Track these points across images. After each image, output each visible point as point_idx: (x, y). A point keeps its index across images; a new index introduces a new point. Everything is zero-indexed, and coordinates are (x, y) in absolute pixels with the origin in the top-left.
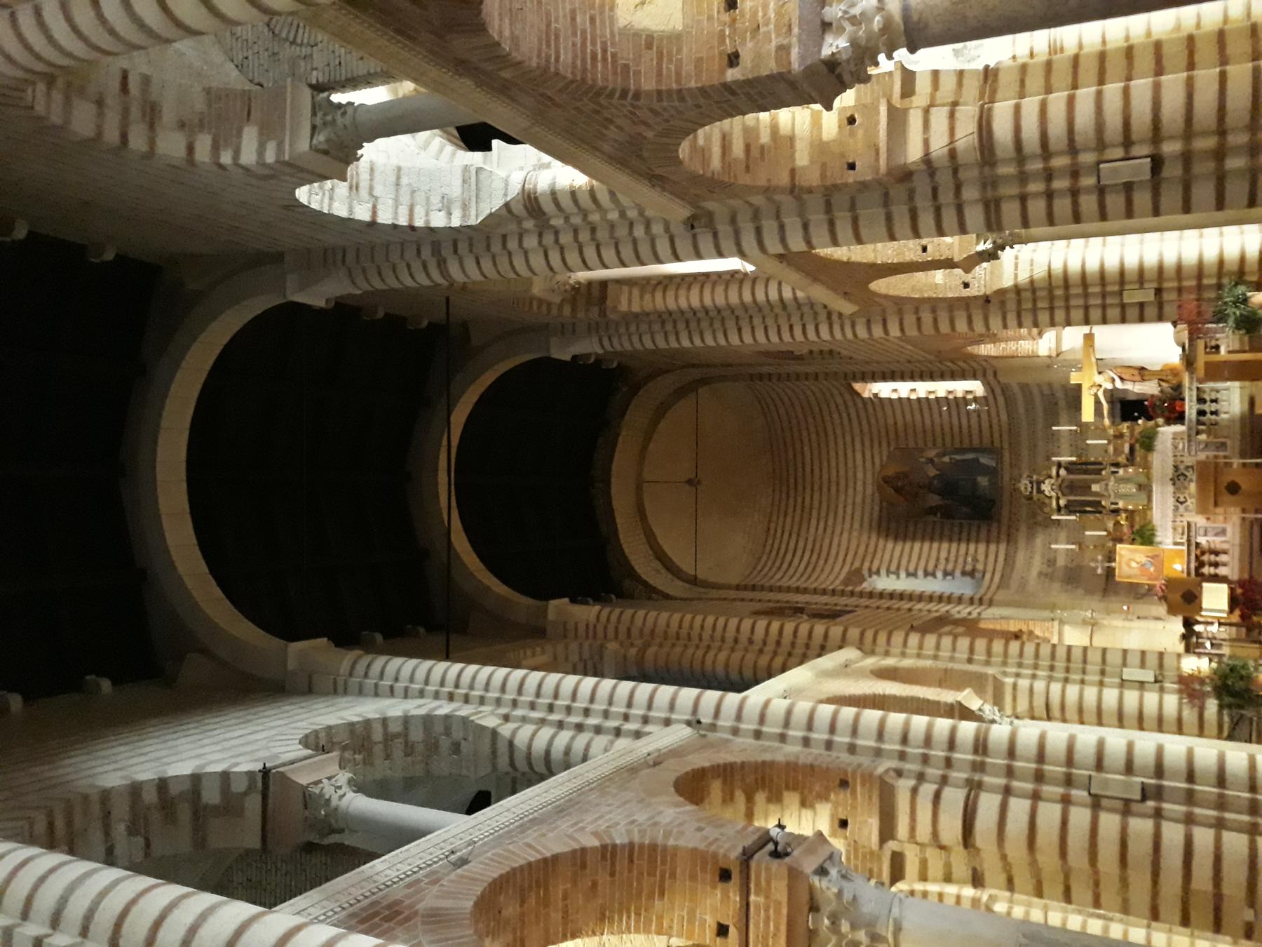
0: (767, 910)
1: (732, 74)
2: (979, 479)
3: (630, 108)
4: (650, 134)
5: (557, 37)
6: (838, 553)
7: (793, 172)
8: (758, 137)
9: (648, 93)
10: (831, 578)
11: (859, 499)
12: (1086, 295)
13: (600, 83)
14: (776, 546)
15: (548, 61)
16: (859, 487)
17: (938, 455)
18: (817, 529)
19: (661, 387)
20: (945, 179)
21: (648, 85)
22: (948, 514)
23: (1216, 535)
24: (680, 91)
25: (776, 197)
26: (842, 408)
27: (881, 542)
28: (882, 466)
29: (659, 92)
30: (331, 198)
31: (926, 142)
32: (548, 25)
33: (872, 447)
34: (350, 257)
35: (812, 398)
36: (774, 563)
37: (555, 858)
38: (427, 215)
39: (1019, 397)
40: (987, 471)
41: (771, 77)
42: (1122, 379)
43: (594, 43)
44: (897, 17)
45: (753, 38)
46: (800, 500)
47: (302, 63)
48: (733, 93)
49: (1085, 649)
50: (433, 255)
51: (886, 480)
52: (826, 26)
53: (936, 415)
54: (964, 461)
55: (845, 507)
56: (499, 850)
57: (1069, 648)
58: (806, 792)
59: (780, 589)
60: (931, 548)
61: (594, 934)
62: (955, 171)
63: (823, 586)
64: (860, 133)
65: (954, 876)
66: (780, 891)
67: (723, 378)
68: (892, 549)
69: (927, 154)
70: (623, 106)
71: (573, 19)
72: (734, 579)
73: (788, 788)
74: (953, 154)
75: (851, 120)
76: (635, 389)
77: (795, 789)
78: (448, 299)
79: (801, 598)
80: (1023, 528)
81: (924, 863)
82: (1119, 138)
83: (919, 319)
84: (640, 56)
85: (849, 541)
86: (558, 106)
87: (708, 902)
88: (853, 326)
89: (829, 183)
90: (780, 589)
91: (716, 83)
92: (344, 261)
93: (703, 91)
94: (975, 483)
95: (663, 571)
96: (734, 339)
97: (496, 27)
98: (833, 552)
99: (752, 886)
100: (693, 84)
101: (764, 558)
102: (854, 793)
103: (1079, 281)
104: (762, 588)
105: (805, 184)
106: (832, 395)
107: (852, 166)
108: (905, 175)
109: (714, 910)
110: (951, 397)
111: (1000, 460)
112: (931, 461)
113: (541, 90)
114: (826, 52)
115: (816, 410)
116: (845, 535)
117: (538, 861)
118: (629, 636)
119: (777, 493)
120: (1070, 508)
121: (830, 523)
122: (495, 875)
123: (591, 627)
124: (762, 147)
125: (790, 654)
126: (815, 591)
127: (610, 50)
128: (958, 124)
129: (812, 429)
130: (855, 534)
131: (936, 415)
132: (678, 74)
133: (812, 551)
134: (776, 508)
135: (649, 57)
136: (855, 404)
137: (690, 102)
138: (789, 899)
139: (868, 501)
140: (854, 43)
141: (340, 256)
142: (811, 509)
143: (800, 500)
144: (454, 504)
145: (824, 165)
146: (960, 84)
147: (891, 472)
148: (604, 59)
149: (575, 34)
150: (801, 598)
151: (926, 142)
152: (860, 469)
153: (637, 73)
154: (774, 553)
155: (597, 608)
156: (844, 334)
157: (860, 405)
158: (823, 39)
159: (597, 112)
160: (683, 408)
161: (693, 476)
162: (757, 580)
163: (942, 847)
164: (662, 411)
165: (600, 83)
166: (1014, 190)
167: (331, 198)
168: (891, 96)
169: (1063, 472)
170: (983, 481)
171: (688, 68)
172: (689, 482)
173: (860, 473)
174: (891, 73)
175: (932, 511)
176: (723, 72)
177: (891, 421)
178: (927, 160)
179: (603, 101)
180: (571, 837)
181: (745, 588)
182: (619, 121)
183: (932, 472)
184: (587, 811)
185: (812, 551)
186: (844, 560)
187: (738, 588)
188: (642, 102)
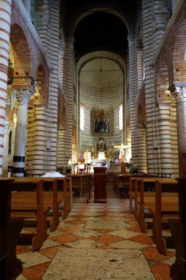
0: (22, 82)
1: (175, 70)
4: (166, 55)
7: (159, 85)
10: (82, 101)
11: (99, 106)
13: (175, 44)
15: (180, 32)
16: (101, 106)
19: (122, 62)
20: (157, 113)
21: (174, 54)
22: (96, 123)
26: (117, 102)
27: (90, 111)
31: (163, 110)
33: (109, 108)
35: (119, 96)
36: (85, 89)
37: (26, 40)
39: (119, 136)
40: (105, 130)
41: (173, 78)
42: (122, 153)
44: (182, 100)
45: (181, 74)
48: (171, 71)
49: (71, 148)
52: (182, 88)
53: (116, 121)
54: (107, 126)
56: (26, 28)
57: (71, 145)
58: (42, 91)
59: (79, 90)
60: (89, 120)
61: (13, 49)
63: (80, 97)
64: (166, 98)
65: (29, 119)
66: (26, 84)
67: (124, 76)
68: (89, 113)
69: (161, 110)
72: (81, 79)
73: (42, 87)
74: (160, 114)
77: (42, 89)
79: (77, 94)
81: (31, 113)
84: (180, 52)
85: (90, 104)
87: (22, 71)
88: (133, 101)
89: (157, 92)
90: (79, 90)
94: (102, 128)
95: (82, 64)
96: (130, 77)
97: (38, 41)
98: (87, 101)
99: (26, 79)
100: (173, 63)
101: (86, 87)
102: (43, 100)
104: (79, 86)
105: (157, 87)
106: (120, 100)
108: (157, 105)
109: (21, 72)
110: (119, 123)
111: (107, 133)
112: (106, 120)
114: (177, 88)
115: (117, 96)
116: (91, 103)
117: (25, 37)
118: (67, 56)
120: (98, 145)
121: (94, 100)
122: (22, 28)
123: (68, 47)
125: (66, 90)
126: (79, 97)
127: (182, 45)
128: (166, 115)
129: (113, 96)
130: (91, 105)
131: (116, 121)
132: (176, 60)
135: (179, 54)
136: (118, 104)
138: (25, 85)
139: (99, 108)
140: (178, 93)
142: (96, 96)
144: (94, 12)
145: (160, 91)
147: (104, 112)
148: (180, 44)
150: (77, 94)
151: (163, 110)
152: (105, 106)
153: (177, 51)
155: (73, 48)
156: (131, 99)
157: (118, 105)
158: (179, 87)
160: (118, 68)
162: (80, 85)
163: (35, 116)
164: (117, 62)
165: (175, 44)
166: (153, 126)
168: (172, 103)
169: (105, 144)
170: (103, 130)
171: (177, 62)
173: (104, 106)
175: (96, 120)
176: (175, 69)
177: (114, 110)
178: (159, 110)
180: (30, 43)
181: (79, 82)
184: (35, 46)
187: (79, 81)
188: (172, 53)
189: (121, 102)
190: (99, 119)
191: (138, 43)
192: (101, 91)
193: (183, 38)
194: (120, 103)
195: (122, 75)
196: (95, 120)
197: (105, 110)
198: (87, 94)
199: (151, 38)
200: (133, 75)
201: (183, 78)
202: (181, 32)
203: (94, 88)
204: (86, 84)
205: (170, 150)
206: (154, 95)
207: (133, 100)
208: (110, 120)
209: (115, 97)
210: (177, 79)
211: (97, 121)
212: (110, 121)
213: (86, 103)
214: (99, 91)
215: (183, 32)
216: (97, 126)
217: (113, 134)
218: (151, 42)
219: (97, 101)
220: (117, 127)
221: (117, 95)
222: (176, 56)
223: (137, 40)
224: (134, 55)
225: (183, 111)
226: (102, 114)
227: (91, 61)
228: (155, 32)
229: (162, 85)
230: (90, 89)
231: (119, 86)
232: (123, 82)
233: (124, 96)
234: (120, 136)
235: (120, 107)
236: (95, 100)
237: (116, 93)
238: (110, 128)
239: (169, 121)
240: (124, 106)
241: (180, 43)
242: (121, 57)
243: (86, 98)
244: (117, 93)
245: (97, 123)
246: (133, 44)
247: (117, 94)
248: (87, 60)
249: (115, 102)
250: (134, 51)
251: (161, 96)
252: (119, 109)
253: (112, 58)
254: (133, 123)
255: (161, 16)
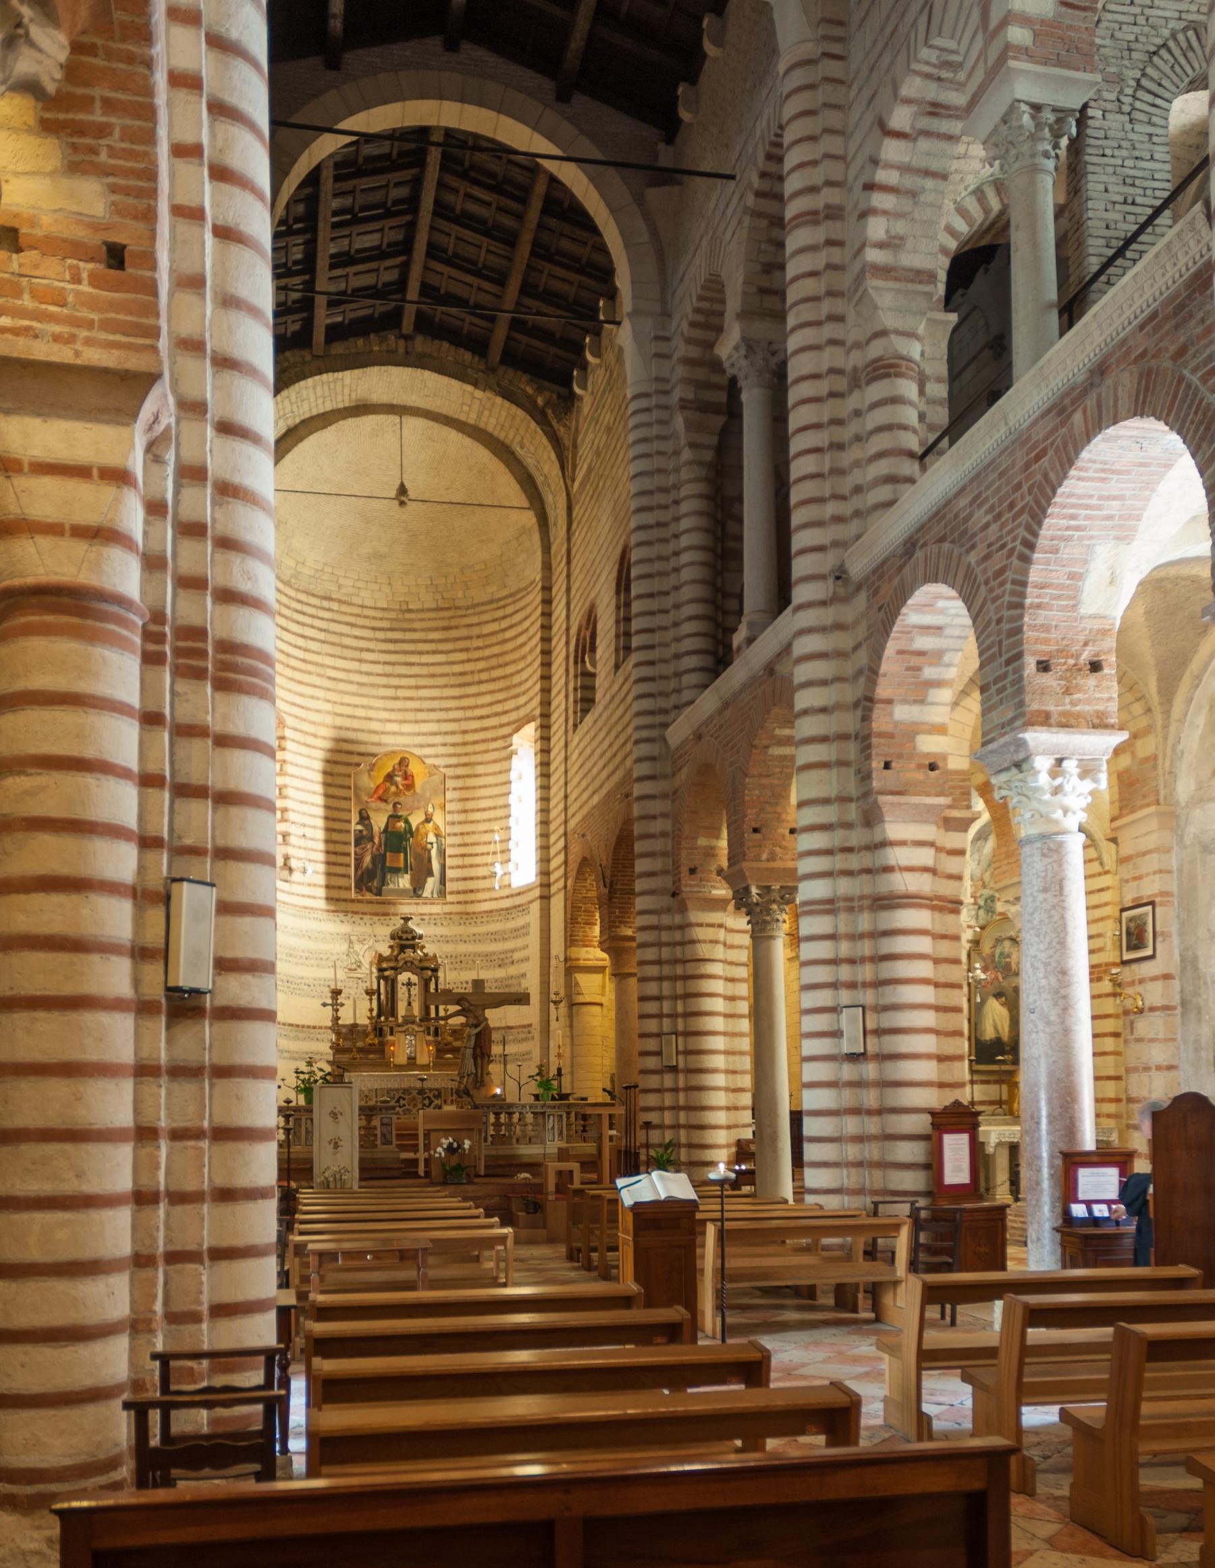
1: (1030, 663)
2: (407, 877)
3: (1010, 546)
4: (973, 558)
5: (1103, 480)
6: (301, 695)
7: (890, 702)
8: (931, 664)
9: (1026, 572)
11: (374, 726)
12: (675, 998)
14: (306, 609)
17: (437, 828)
18: (335, 668)
23: (383, 1135)
24: (1021, 606)
25: (862, 680)
26: (498, 708)
28: (420, 758)
29: (1024, 584)
30: (928, 76)
31: (903, 843)
32: (1113, 472)
33: (445, 745)
34: (834, 68)
38: (885, 213)
39: (511, 925)
43: (1087, 518)
46: (371, 645)
47: (1113, 96)
48: (1008, 662)
50: (827, 206)
51: (403, 762)
55: (363, 707)
62: (868, 871)
70: (1014, 540)
71: (1115, 498)
75: (932, 767)
76: (540, 417)
78: (732, 177)
80: (345, 928)
82: (691, 1047)
83: (654, 817)
85: (318, 711)
86: (1027, 466)
89: (874, 740)
91: (1025, 646)
92: (826, 55)
93: (1018, 630)
94: (396, 871)
100: (1026, 619)
101: (292, 593)
103: (690, 990)
107: (887, 766)
108: (871, 818)
112: (428, 820)
113: (1051, 453)
116: (328, 707)
119: (379, 614)
124: (919, 669)
127: (1077, 534)
128: (917, 874)
133: (304, 661)
134: (358, 611)
137: (1006, 613)
141: (836, 48)
143: (371, 645)
145: (891, 736)
146: (951, 877)
147: (414, 768)
148: (1068, 528)
149: (1100, 498)
151: (903, 843)
154: (299, 607)
159: (1012, 506)
160: (509, 489)
161: (412, 494)
167: (928, 76)
170: (404, 882)
172: (402, 490)
174: (969, 807)
175: (364, 818)
179: (1025, 517)
182: (994, 527)
183: (416, 820)
185: (304, 661)
186: (294, 704)
188: (1015, 561)
189: (522, 712)
190: (378, 810)
191: (688, 381)
192: (392, 629)
193: (1091, 497)
194: (513, 716)
195: (536, 537)
196: (355, 818)
197: (417, 751)
198: (301, 642)
199: (844, 408)
200: (656, 580)
201: (1068, 707)
202: (1086, 470)
203: (344, 608)
204: (297, 575)
205: (933, 1064)
206: (851, 750)
207: (654, 733)
208: (449, 818)
209: (484, 676)
210: (1039, 712)
211: (369, 827)
212: (449, 829)
213: (298, 700)
214: (374, 629)
215: (1096, 471)
216: (367, 859)
217: (470, 908)
218: (845, 434)
219: (365, 690)
220: (498, 869)
221: (494, 662)
222: (1043, 586)
223: (687, 361)
224: (660, 453)
225: (1061, 888)
226: (398, 779)
227: (333, 427)
228: (868, 384)
229: (905, 702)
230: (322, 614)
231: (510, 610)
232: (544, 588)
233: (546, 677)
234: (520, 922)
235: (516, 739)
236: (354, 688)
237: (487, 652)
238: (450, 874)
239: (933, 908)
240: (545, 738)
241: (1073, 523)
242: (533, 424)
243: (294, 668)
244: (496, 650)
245: (371, 839)
246: (658, 379)
247: (502, 660)
248: (307, 415)
249: (482, 706)
250: (665, 423)
251: (893, 765)
252: (509, 758)
253: (471, 421)
254: (652, 874)
255: (899, 291)
